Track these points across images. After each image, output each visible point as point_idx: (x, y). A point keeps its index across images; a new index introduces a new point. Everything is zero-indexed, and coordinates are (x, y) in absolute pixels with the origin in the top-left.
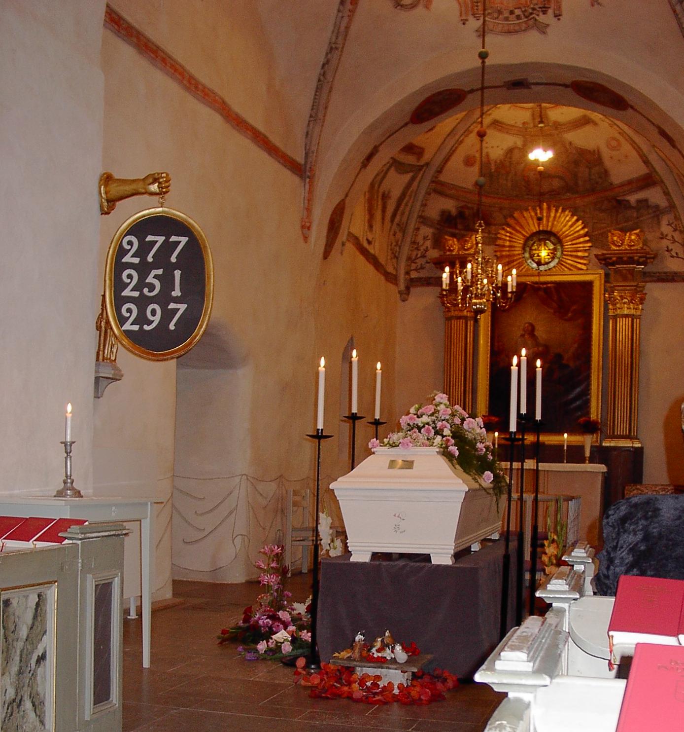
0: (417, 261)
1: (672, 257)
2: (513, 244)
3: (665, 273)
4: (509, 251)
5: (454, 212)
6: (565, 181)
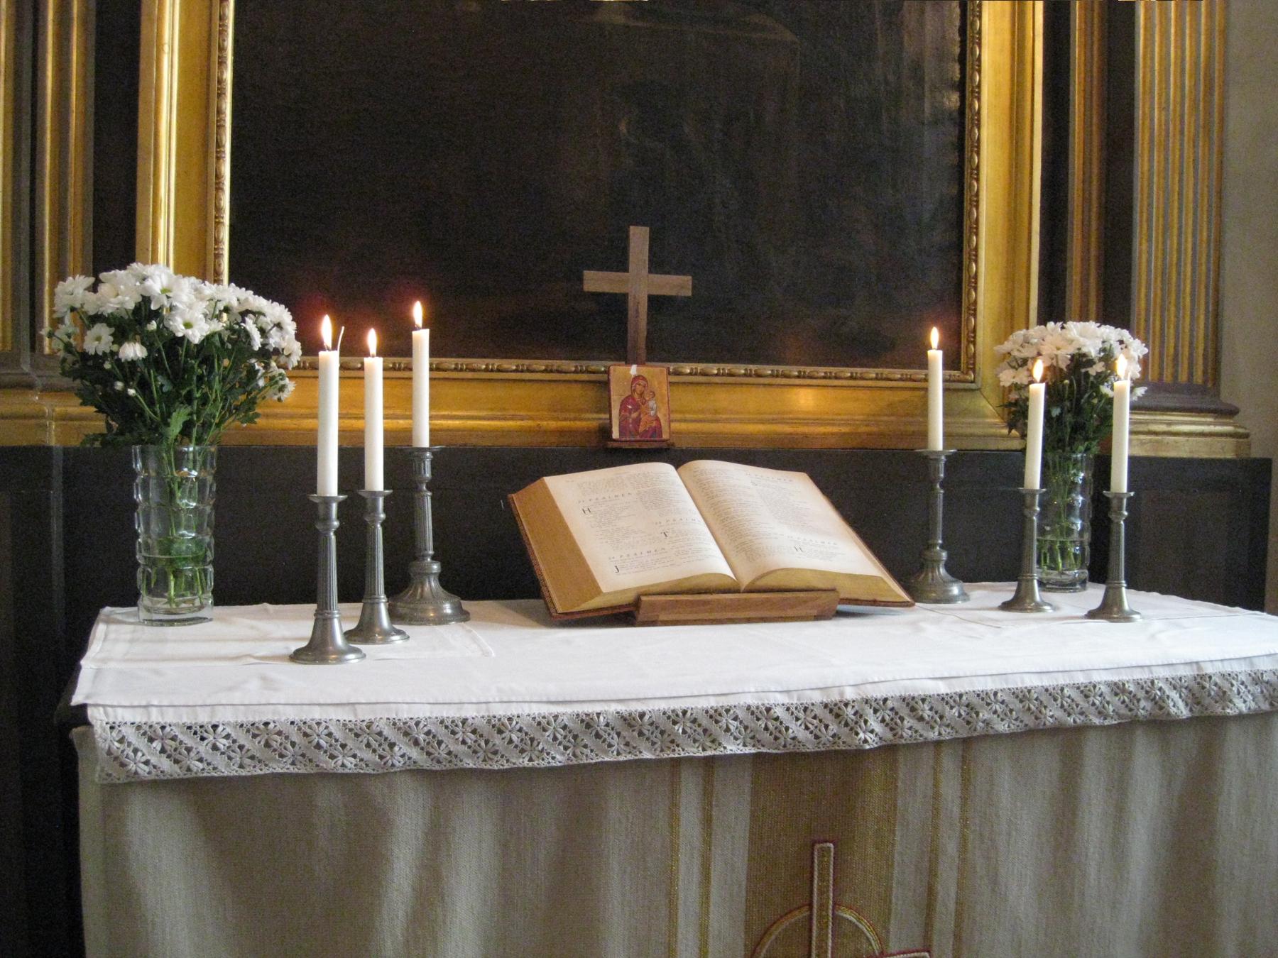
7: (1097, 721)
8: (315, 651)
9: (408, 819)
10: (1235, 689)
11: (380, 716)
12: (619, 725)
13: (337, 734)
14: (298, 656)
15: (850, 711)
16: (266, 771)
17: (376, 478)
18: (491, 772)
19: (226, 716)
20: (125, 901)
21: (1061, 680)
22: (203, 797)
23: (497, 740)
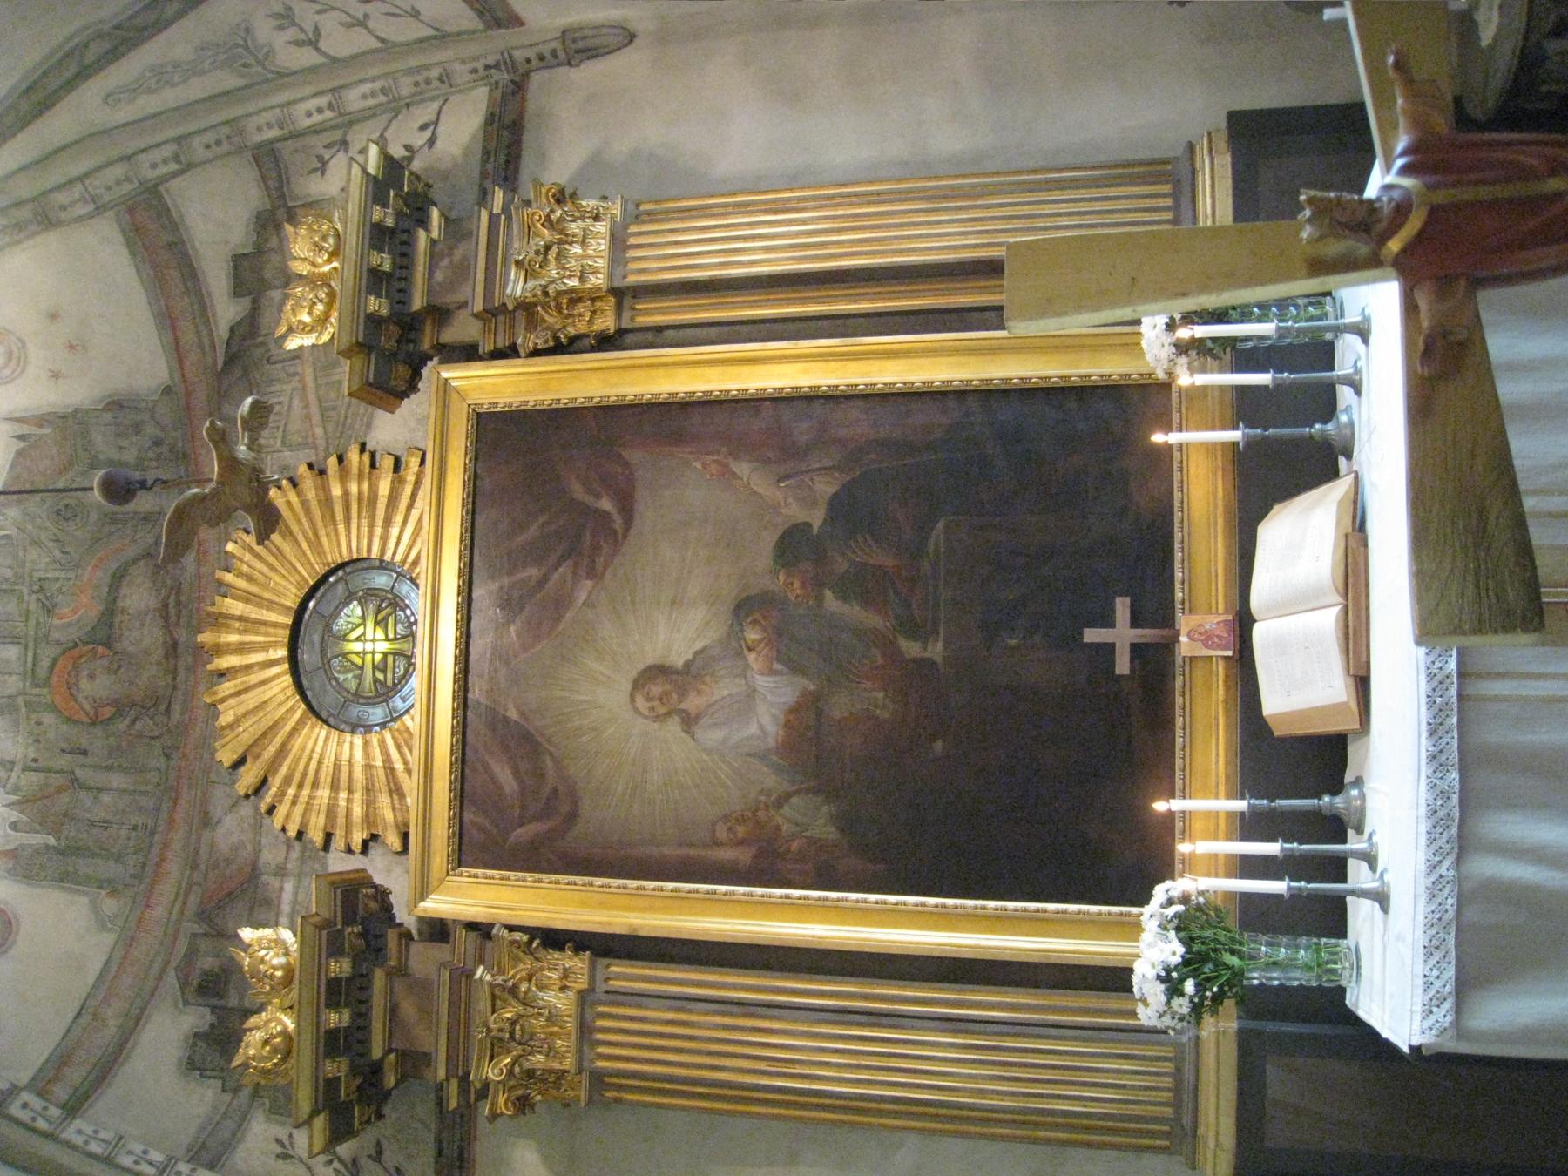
1: (432, 141)
2: (326, 777)
3: (486, 154)
4: (350, 791)
5: (197, 1018)
6: (135, 561)
8: (1382, 899)
11: (1424, 882)
14: (1385, 909)
17: (1272, 848)
19: (1420, 968)
20: (1529, 1034)
22: (1466, 987)
23: (1441, 814)
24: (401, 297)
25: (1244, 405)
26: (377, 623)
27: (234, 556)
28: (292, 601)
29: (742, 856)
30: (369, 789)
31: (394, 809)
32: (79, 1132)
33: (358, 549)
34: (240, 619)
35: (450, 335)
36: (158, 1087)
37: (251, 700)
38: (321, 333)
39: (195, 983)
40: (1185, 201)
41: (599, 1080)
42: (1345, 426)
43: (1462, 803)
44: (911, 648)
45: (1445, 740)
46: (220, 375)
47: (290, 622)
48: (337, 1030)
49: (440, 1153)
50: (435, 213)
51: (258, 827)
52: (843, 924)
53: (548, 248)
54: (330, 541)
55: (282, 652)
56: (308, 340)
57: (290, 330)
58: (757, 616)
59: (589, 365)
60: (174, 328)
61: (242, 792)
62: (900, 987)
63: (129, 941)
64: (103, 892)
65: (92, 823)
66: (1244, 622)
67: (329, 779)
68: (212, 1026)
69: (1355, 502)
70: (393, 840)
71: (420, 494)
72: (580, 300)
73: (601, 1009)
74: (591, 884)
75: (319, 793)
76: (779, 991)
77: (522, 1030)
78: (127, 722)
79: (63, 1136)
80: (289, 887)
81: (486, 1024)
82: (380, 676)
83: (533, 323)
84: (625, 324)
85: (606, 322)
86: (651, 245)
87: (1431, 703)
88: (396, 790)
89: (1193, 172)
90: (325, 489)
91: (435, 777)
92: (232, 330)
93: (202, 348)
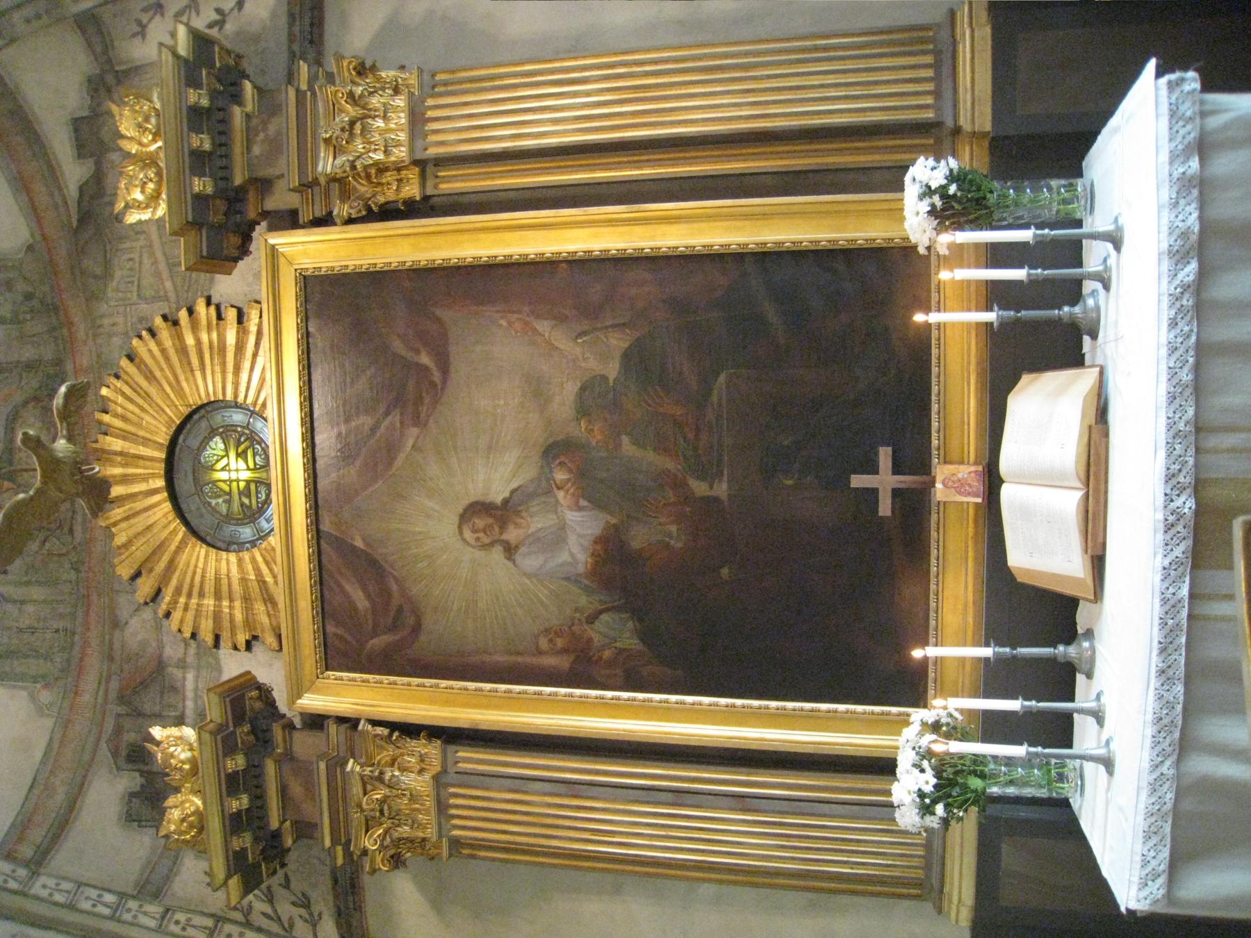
0: (285, 919)
2: (209, 587)
3: (291, 16)
4: (231, 600)
5: (129, 781)
7: (1193, 338)
8: (1108, 763)
9: (1205, 766)
10: (1181, 224)
11: (1147, 778)
12: (1164, 655)
13: (1153, 800)
15: (1171, 518)
16: (1169, 835)
18: (1188, 627)
20: (1231, 902)
21: (1164, 367)
23: (1165, 721)
24: (222, 175)
25: (995, 294)
26: (238, 455)
27: (109, 400)
28: (163, 438)
29: (562, 663)
30: (247, 599)
31: (269, 615)
32: (44, 886)
33: (215, 393)
34: (121, 454)
35: (271, 204)
36: (103, 842)
37: (140, 523)
38: (155, 208)
39: (124, 754)
40: (946, 71)
41: (456, 843)
42: (1092, 310)
43: (1185, 709)
44: (699, 488)
45: (1174, 657)
46: (76, 232)
47: (164, 456)
48: (239, 812)
49: (336, 881)
50: (248, 86)
51: (158, 627)
52: (651, 720)
53: (352, 123)
54: (187, 380)
55: (160, 483)
56: (146, 216)
57: (127, 207)
58: (562, 459)
59: (400, 232)
60: (28, 191)
61: (142, 601)
62: (698, 770)
63: (65, 724)
64: (38, 686)
65: (20, 630)
66: (992, 481)
67: (212, 590)
68: (142, 786)
69: (1099, 395)
70: (271, 640)
71: (261, 352)
72: (387, 169)
73: (452, 790)
74: (437, 686)
75: (205, 602)
76: (598, 772)
77: (390, 808)
78: (37, 543)
79: (32, 892)
80: (190, 677)
81: (359, 806)
82: (246, 501)
83: (346, 195)
84: (429, 192)
85: (412, 190)
86: (448, 118)
87: (1164, 624)
88: (269, 600)
89: (954, 44)
90: (180, 337)
91: (299, 596)
92: (81, 189)
93: (56, 206)
